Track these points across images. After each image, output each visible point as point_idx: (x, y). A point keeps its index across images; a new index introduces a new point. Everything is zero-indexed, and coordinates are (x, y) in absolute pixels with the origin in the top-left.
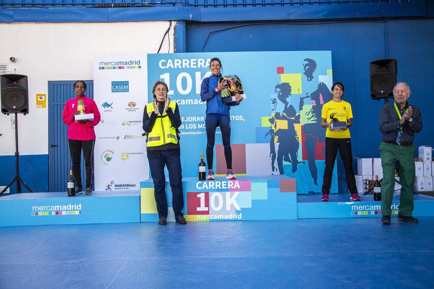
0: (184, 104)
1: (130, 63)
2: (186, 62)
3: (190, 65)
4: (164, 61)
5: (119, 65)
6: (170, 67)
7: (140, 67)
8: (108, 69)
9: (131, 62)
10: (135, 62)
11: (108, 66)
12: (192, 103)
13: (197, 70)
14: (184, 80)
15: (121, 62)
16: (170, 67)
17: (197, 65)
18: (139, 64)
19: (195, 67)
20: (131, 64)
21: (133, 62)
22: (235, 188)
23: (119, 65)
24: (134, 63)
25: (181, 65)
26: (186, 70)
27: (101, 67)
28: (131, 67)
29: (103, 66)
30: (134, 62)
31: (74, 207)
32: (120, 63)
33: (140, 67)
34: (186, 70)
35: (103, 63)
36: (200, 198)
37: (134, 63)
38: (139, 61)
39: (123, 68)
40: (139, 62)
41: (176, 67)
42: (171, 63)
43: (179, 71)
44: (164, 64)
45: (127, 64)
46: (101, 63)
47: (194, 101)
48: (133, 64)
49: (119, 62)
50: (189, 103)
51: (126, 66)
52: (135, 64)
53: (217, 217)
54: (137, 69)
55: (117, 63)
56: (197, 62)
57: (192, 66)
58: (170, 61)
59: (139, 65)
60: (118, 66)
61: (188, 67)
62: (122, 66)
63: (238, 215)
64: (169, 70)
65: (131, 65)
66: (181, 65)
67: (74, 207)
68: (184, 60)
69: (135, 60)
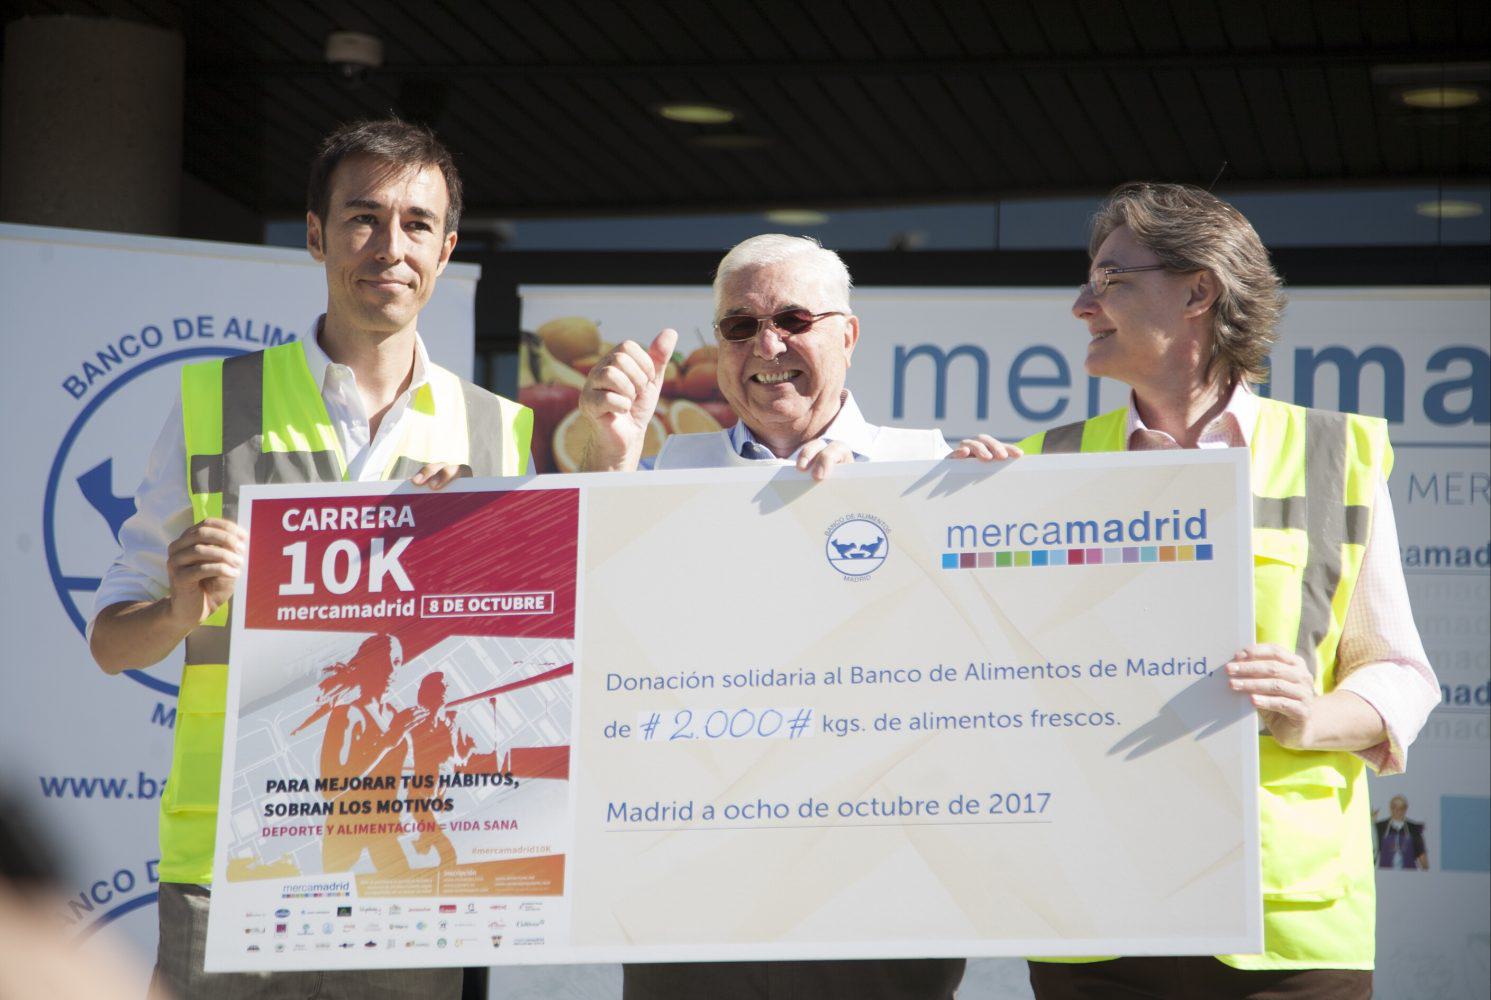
0: (337, 616)
1: (1139, 530)
2: (350, 514)
3: (358, 521)
4: (296, 512)
5: (1069, 540)
6: (309, 528)
7: (1204, 553)
8: (999, 564)
9: (1146, 523)
10: (1176, 521)
11: (1002, 548)
12: (357, 615)
13: (376, 532)
14: (342, 558)
15: (1081, 526)
16: (309, 528)
17: (376, 520)
18: (1203, 534)
19: (372, 526)
20: (1146, 536)
21: (1159, 523)
22: (399, 524)
23: (1069, 540)
24: (1168, 529)
25: (338, 521)
26: (348, 534)
27: (955, 555)
28: (1149, 555)
29: (968, 549)
30: (1166, 521)
31: (394, 610)
32: (1076, 530)
33: (1204, 553)
34: (348, 534)
35: (969, 533)
36: (290, 558)
37: (1168, 529)
38: (1198, 516)
39: (1096, 556)
40: (1202, 521)
41: (324, 527)
42: (314, 517)
43: (331, 536)
44: (294, 520)
45: (1120, 538)
46: (956, 534)
47: (361, 610)
48: (1159, 537)
49: (1070, 526)
50: (350, 615)
51: (1117, 545)
52: (1176, 536)
53: (386, 612)
54: (1190, 568)
55: (1057, 532)
56: (376, 514)
57: (364, 525)
58: (310, 512)
59: (1201, 541)
60: (1066, 547)
61: (354, 526)
62: (1089, 545)
63: (403, 603)
64: (308, 535)
65: (1143, 544)
66: (338, 521)
67: (394, 610)
68: (345, 511)
69: (1176, 512)
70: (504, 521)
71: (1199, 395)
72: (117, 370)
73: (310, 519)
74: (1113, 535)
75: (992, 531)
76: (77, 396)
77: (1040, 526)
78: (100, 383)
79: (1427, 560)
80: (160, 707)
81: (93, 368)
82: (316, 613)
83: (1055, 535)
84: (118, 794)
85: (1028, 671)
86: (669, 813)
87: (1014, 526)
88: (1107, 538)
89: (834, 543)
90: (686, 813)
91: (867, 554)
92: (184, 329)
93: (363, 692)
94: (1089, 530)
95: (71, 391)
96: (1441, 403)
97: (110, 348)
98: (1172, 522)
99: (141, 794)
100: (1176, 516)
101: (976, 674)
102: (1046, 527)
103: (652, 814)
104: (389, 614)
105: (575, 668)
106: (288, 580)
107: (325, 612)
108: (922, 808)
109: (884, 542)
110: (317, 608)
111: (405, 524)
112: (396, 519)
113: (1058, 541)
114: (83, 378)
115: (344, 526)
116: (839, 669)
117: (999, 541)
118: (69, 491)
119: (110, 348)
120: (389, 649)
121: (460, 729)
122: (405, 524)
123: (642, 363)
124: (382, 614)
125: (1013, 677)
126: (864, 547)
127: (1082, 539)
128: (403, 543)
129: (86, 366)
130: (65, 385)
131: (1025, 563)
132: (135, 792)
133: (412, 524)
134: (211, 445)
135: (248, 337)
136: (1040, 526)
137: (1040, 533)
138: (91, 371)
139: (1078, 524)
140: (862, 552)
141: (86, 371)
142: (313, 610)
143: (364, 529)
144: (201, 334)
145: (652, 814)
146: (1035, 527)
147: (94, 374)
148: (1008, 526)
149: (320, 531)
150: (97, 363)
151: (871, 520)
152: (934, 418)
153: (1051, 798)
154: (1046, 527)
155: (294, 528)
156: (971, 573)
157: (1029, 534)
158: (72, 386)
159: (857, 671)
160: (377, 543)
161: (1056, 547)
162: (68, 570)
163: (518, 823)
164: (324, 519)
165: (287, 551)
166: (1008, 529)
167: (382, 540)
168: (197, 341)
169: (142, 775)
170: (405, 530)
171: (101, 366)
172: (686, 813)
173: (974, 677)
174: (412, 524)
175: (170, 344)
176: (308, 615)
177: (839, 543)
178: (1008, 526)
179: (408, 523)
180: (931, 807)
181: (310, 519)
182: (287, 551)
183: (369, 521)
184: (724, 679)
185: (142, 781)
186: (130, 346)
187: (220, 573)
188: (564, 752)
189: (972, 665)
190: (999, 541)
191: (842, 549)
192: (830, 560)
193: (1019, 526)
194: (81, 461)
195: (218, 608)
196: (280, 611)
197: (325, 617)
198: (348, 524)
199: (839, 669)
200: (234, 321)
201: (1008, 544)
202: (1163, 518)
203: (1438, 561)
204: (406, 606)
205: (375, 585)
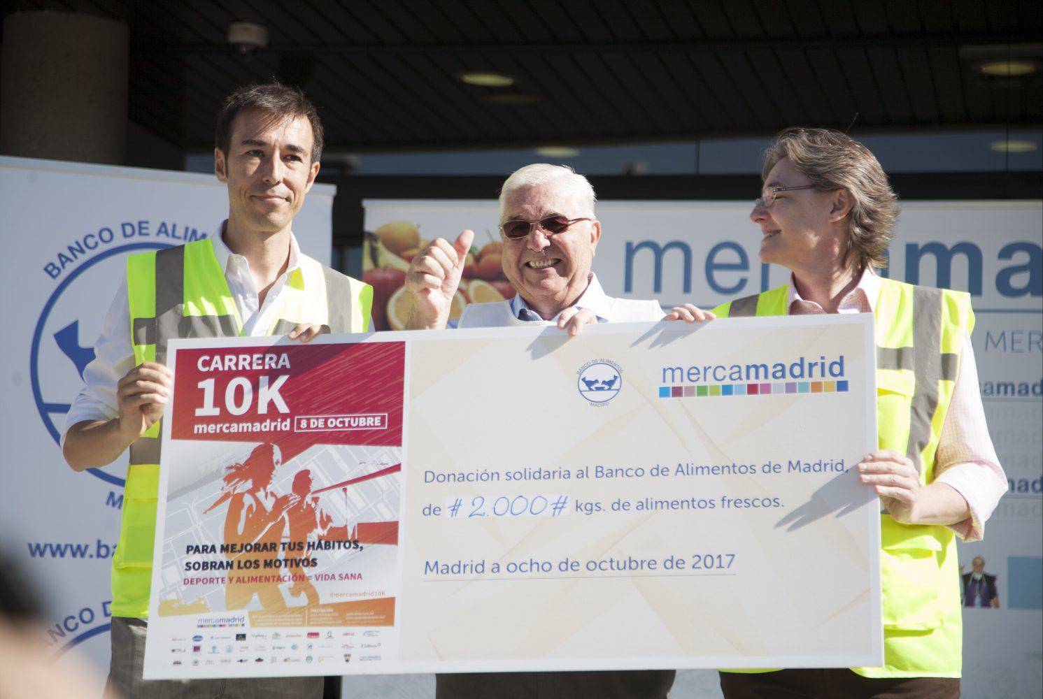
0: (236, 431)
1: (797, 370)
2: (245, 360)
3: (251, 364)
4: (207, 358)
5: (748, 377)
6: (216, 369)
7: (842, 386)
8: (699, 394)
9: (801, 366)
10: (823, 364)
11: (701, 383)
12: (250, 430)
13: (263, 372)
14: (239, 390)
15: (756, 367)
16: (216, 369)
17: (263, 364)
18: (841, 373)
19: (261, 367)
20: (802, 375)
21: (811, 366)
22: (279, 367)
23: (748, 377)
24: (817, 370)
25: (237, 364)
26: (243, 373)
27: (668, 388)
28: (804, 388)
29: (677, 383)
30: (816, 364)
31: (276, 427)
32: (753, 371)
33: (842, 386)
34: (243, 373)
35: (678, 373)
36: (203, 390)
37: (817, 370)
38: (838, 361)
39: (766, 389)
40: (841, 364)
41: (226, 369)
42: (219, 362)
43: (231, 374)
44: (206, 364)
45: (783, 376)
46: (669, 373)
47: (253, 426)
48: (810, 375)
49: (748, 368)
50: (245, 430)
51: (782, 381)
52: (823, 375)
53: (270, 428)
54: (832, 397)
55: (739, 372)
56: (263, 359)
57: (255, 367)
58: (217, 358)
59: (840, 379)
60: (746, 382)
61: (248, 368)
62: (761, 381)
63: (282, 422)
64: (215, 374)
65: (799, 380)
66: (237, 364)
67: (276, 427)
68: (241, 357)
69: (823, 358)
70: (353, 364)
71: (839, 276)
72: (82, 258)
73: (217, 363)
74: (779, 374)
75: (694, 371)
76: (54, 277)
77: (728, 368)
78: (70, 267)
79: (999, 392)
80: (112, 494)
81: (65, 257)
82: (221, 428)
83: (738, 374)
84: (82, 555)
85: (719, 469)
86: (468, 568)
87: (710, 367)
88: (774, 376)
89: (584, 380)
90: (480, 568)
91: (607, 387)
92: (128, 230)
93: (254, 484)
94: (762, 370)
95: (50, 273)
96: (1008, 282)
97: (77, 243)
98: (820, 365)
99: (99, 555)
100: (823, 361)
101: (683, 471)
102: (731, 368)
103: (456, 569)
104: (272, 429)
105: (403, 467)
106: (201, 405)
107: (227, 428)
108: (645, 565)
109: (618, 379)
110: (221, 425)
111: (284, 367)
112: (277, 363)
113: (740, 378)
114: (58, 264)
115: (240, 368)
116: (587, 468)
117: (698, 378)
118: (48, 343)
119: (77, 243)
120: (272, 454)
121: (321, 510)
122: (284, 367)
123: (449, 254)
124: (268, 429)
125: (709, 473)
126: (604, 382)
127: (757, 377)
128: (282, 380)
129: (60, 256)
130: (46, 269)
131: (717, 394)
132: (95, 554)
133: (288, 366)
134: (148, 311)
135: (174, 236)
136: (728, 368)
137: (728, 372)
138: (64, 259)
139: (754, 366)
140: (603, 386)
141: (61, 260)
142: (219, 426)
143: (255, 370)
144: (140, 234)
145: (456, 569)
146: (724, 368)
147: (66, 262)
148: (705, 368)
149: (224, 371)
150: (68, 254)
151: (609, 363)
152: (653, 292)
153: (735, 558)
154: (731, 368)
155: (206, 369)
156: (679, 400)
157: (720, 373)
158: (50, 270)
159: (599, 469)
160: (264, 380)
161: (738, 382)
162: (47, 398)
163: (362, 575)
164: (227, 363)
165: (201, 385)
166: (705, 370)
167: (267, 378)
168: (137, 239)
169: (99, 541)
170: (283, 371)
171: (70, 256)
172: (480, 568)
173: (682, 473)
174: (288, 366)
175: (119, 241)
176: (216, 430)
177: (587, 379)
178: (705, 368)
179: (285, 366)
180: (651, 564)
181: (217, 363)
182: (201, 385)
183: (258, 365)
184: (507, 474)
185: (99, 546)
186: (91, 242)
187: (154, 401)
188: (394, 525)
189: (680, 465)
190: (698, 378)
191: (589, 384)
192: (581, 391)
193: (713, 368)
194: (56, 322)
195: (153, 425)
196: (196, 427)
197: (228, 431)
198: (243, 366)
199: (587, 468)
200: (163, 224)
201: (705, 380)
202: (813, 362)
203: (1006, 392)
204: (284, 424)
205: (262, 409)
